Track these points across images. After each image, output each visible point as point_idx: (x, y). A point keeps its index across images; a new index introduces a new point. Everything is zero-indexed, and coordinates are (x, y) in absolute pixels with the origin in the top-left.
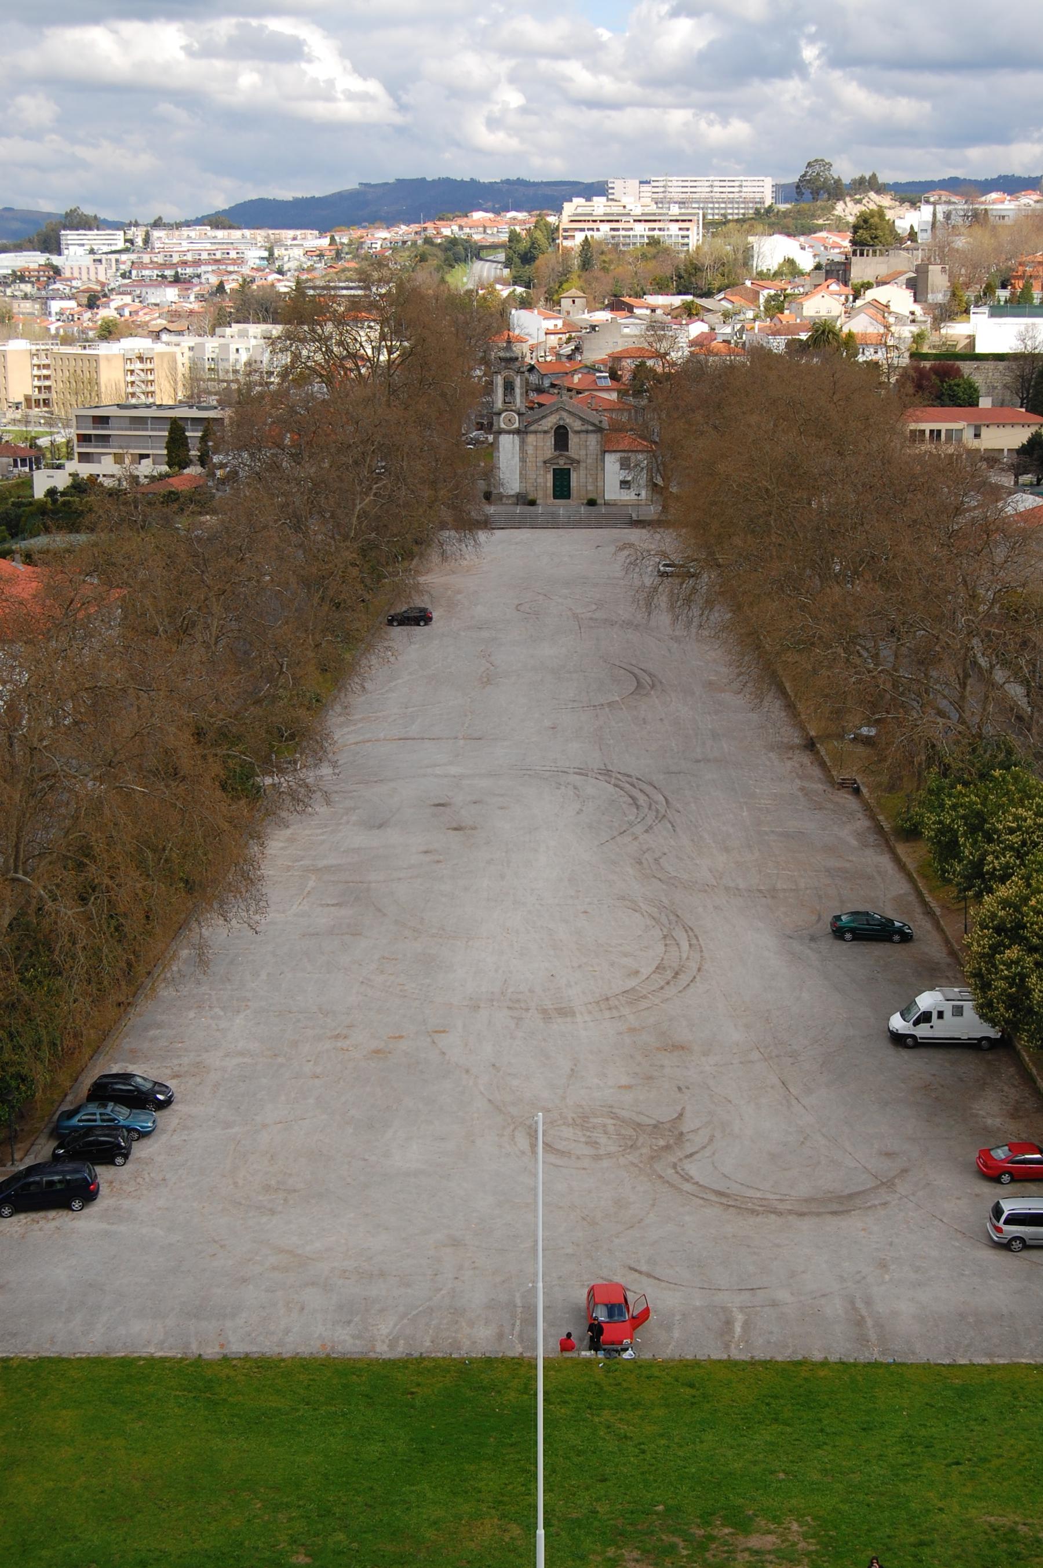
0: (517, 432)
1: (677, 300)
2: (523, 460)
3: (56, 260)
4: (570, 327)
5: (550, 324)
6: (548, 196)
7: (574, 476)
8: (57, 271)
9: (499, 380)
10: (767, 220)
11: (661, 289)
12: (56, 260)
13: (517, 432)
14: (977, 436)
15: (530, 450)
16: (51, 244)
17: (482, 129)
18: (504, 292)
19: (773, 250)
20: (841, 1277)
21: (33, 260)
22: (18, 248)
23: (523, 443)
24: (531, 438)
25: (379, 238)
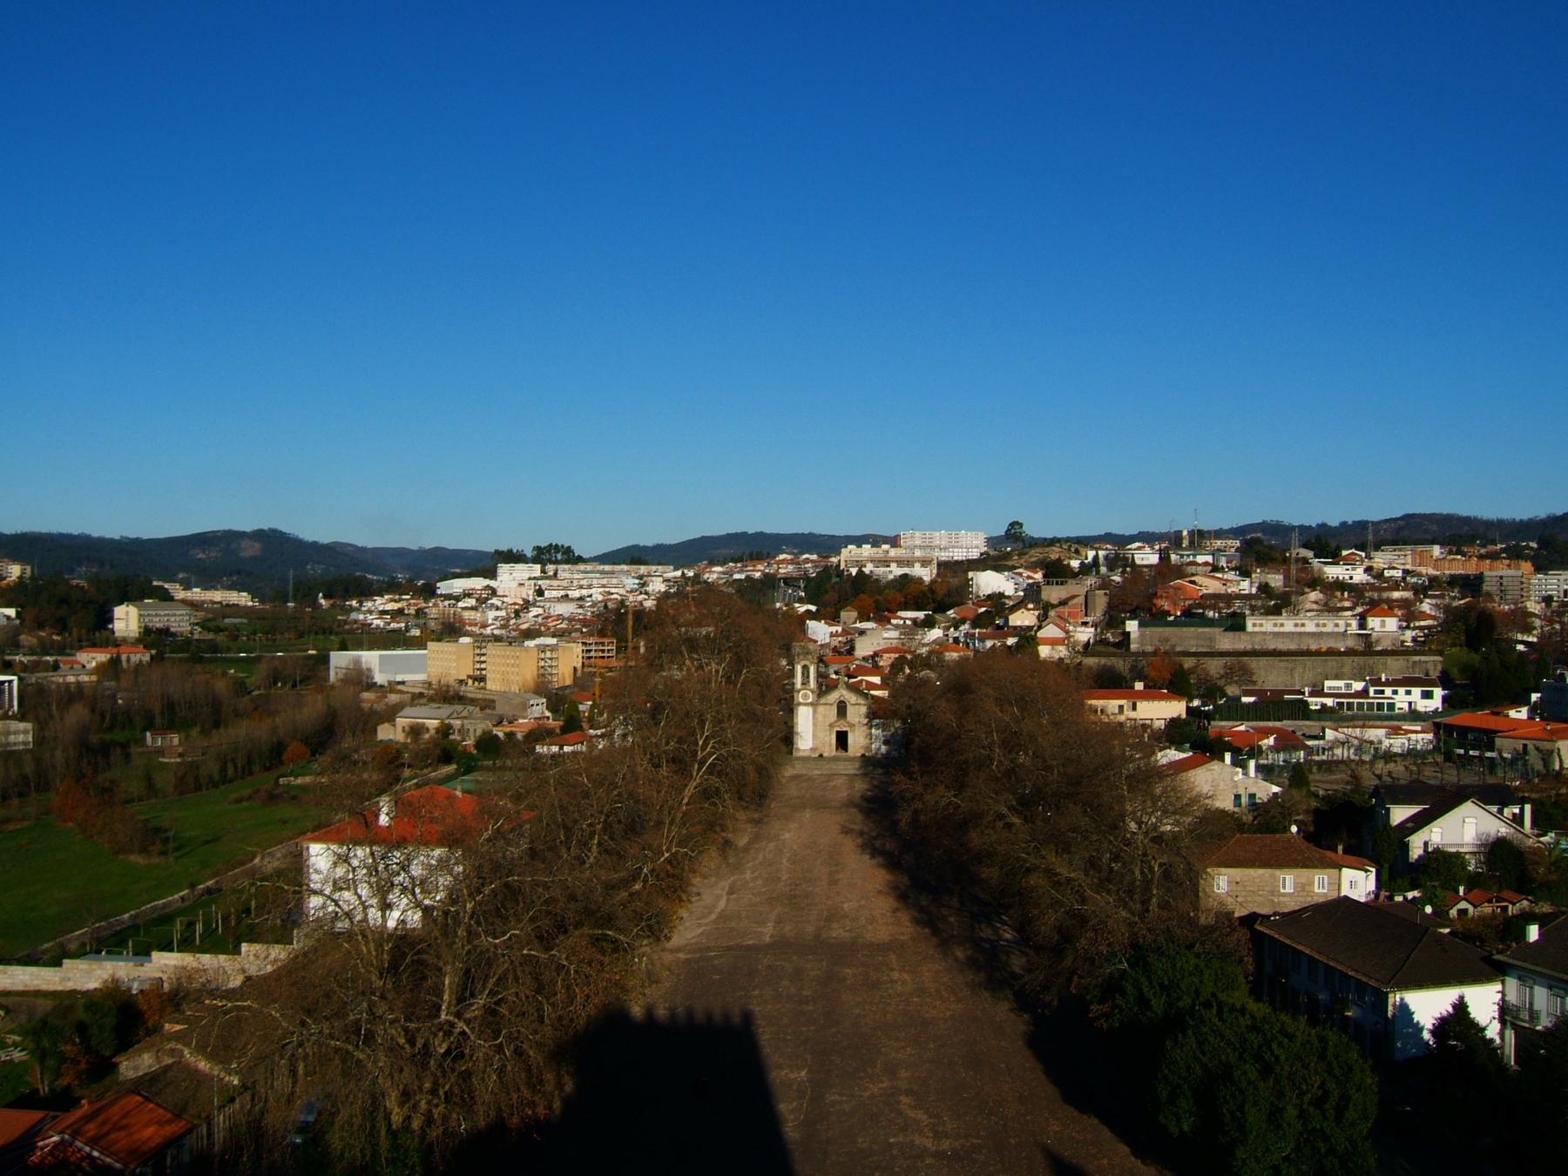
0: (812, 704)
1: (921, 615)
2: (815, 725)
3: (492, 583)
4: (845, 632)
5: (834, 629)
6: (831, 545)
7: (850, 736)
8: (494, 592)
9: (799, 669)
10: (983, 563)
11: (906, 607)
12: (492, 583)
13: (812, 704)
14: (1134, 708)
15: (820, 718)
16: (491, 574)
17: (1427, 702)
18: (802, 608)
19: (989, 582)
20: (634, 827)
21: (478, 583)
22: (469, 575)
23: (815, 712)
24: (821, 709)
25: (714, 574)
